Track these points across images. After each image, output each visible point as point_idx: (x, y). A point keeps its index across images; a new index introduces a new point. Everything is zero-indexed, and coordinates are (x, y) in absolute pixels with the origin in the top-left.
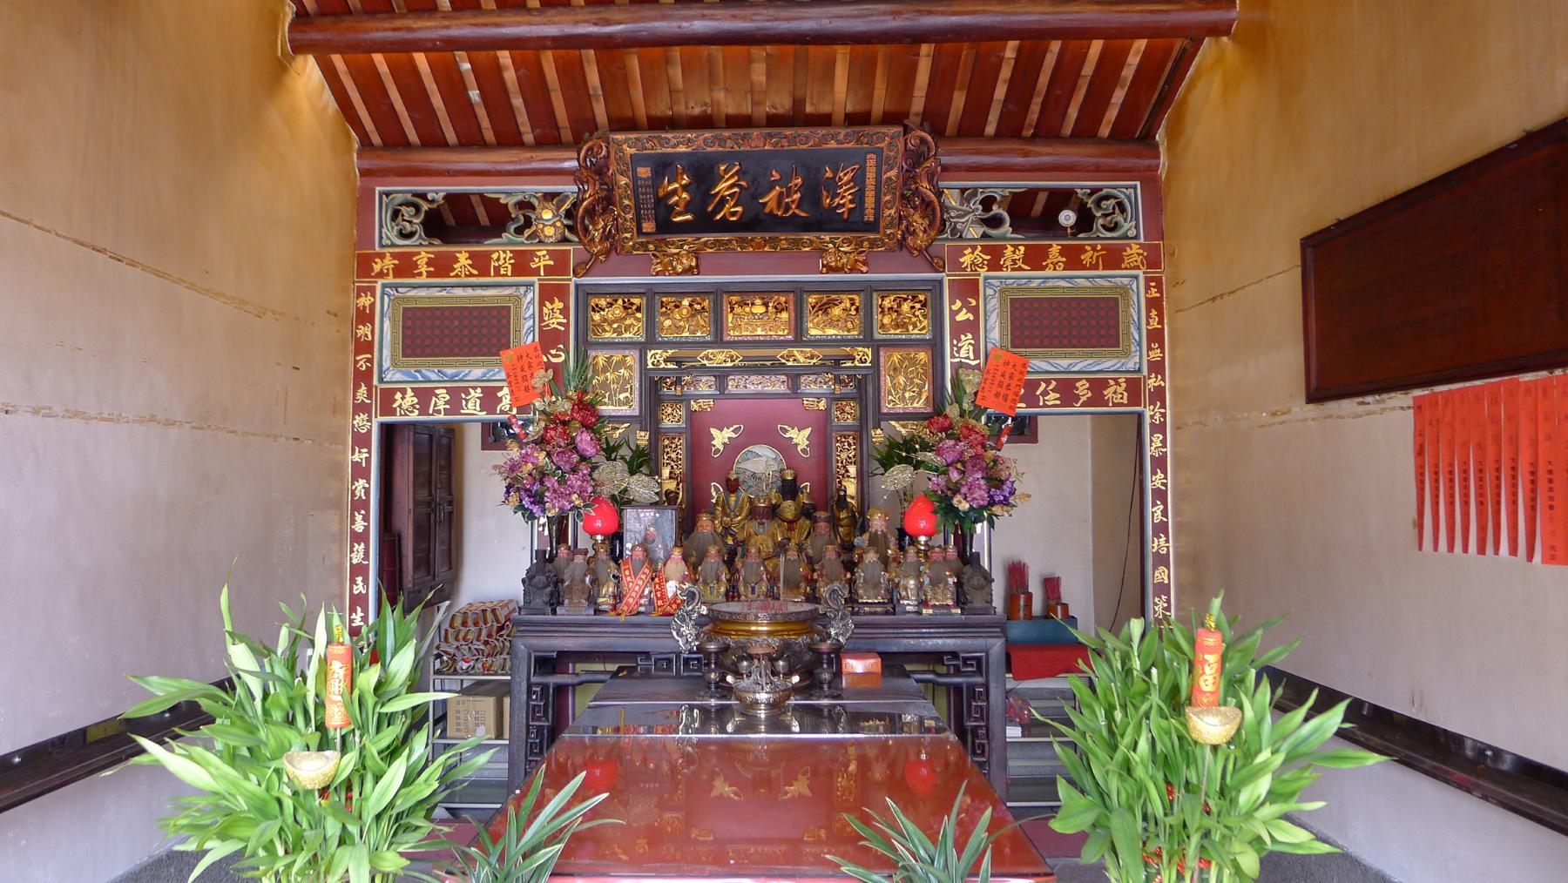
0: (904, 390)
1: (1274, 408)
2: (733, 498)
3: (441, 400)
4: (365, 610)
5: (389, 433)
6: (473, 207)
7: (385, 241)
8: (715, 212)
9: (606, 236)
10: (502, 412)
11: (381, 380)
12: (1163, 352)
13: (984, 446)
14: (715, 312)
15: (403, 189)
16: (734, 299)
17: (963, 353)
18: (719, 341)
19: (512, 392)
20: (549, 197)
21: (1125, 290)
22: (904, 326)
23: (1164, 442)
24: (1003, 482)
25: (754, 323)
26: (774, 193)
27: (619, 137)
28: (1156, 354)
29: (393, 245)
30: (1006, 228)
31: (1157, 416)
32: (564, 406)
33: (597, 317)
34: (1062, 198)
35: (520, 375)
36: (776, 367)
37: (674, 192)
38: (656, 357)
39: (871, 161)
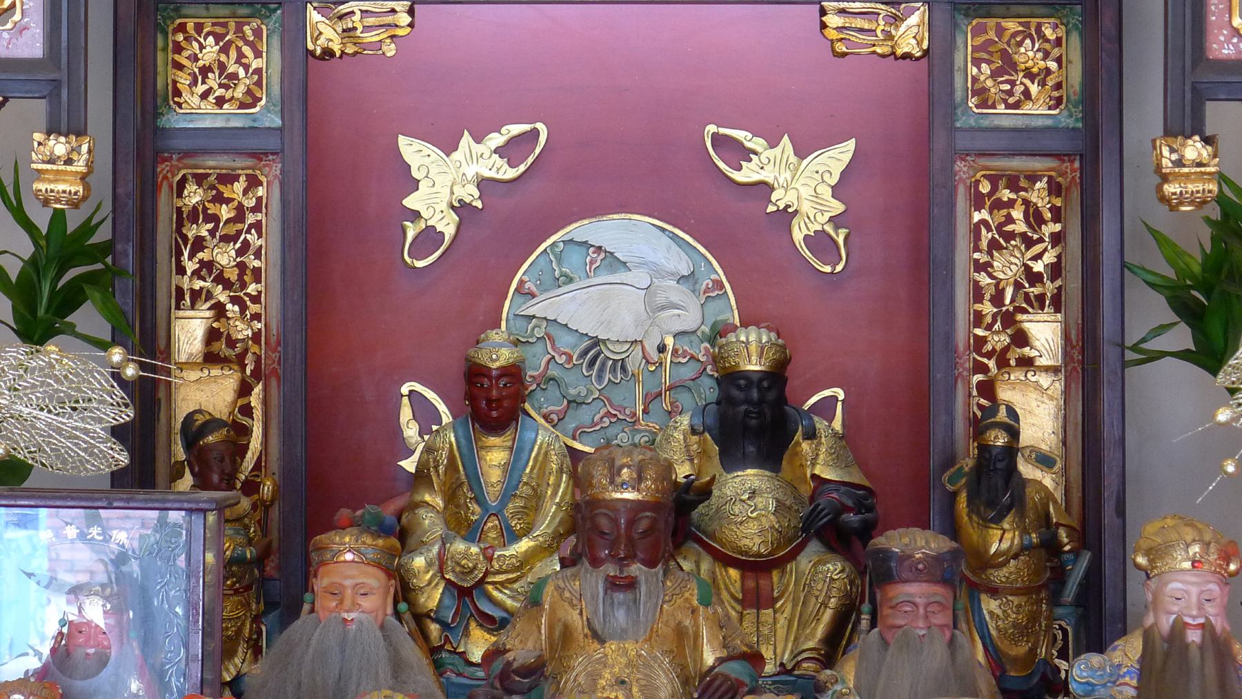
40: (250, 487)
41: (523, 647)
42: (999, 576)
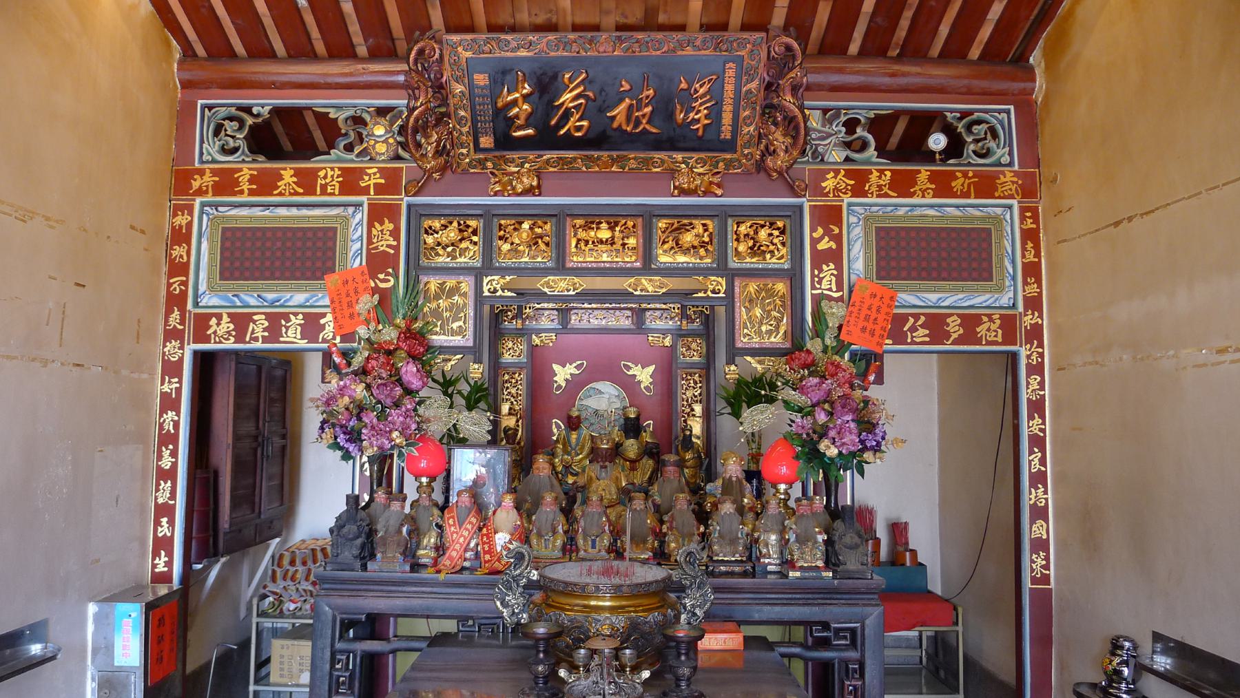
0: (761, 323)
1: (1223, 344)
2: (574, 436)
3: (259, 327)
4: (170, 554)
5: (206, 364)
6: (310, 132)
7: (205, 157)
8: (559, 125)
9: (438, 153)
10: (324, 341)
11: (196, 304)
12: (1040, 286)
13: (852, 387)
15: (227, 102)
16: (579, 222)
17: (825, 284)
18: (561, 267)
19: (335, 318)
20: (382, 112)
21: (998, 220)
23: (1042, 385)
24: (875, 426)
25: (596, 250)
26: (623, 106)
27: (455, 38)
28: (1032, 289)
29: (214, 161)
30: (871, 152)
31: (1034, 357)
32: (389, 334)
33: (430, 240)
34: (923, 123)
35: (345, 300)
37: (514, 103)
38: (493, 283)
39: (731, 71)
40: (519, 443)
41: (582, 481)
42: (688, 464)
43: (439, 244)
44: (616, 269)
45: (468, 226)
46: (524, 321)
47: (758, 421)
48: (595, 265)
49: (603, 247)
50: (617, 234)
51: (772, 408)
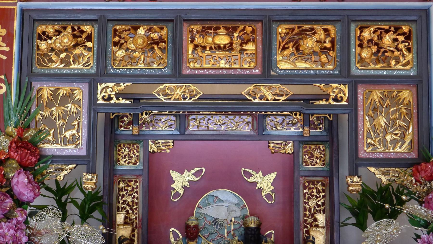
0: (386, 132)
14: (174, 43)
16: (196, 27)
18: (177, 75)
22: (386, 60)
33: (43, 46)
36: (234, 107)
38: (106, 90)
43: (52, 50)
44: (234, 76)
45: (82, 32)
46: (140, 127)
47: (382, 237)
48: (212, 72)
49: (221, 53)
50: (235, 40)
51: (395, 223)
